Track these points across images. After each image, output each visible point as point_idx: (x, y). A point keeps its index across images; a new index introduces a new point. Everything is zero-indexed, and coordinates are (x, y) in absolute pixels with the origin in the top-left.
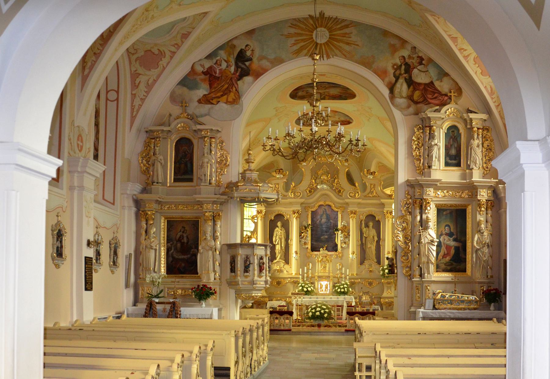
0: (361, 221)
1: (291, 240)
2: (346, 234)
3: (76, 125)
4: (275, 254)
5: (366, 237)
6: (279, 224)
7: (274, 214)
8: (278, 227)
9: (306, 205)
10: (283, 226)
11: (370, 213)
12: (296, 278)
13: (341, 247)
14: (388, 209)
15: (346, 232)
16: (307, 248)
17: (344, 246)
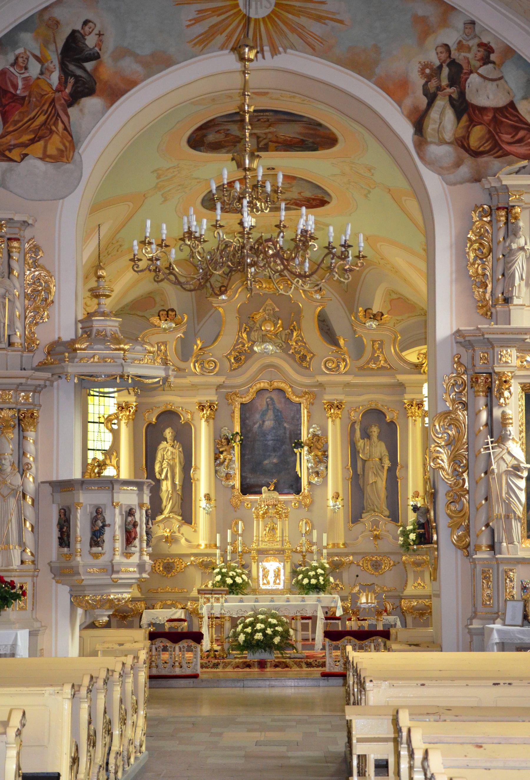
1: (197, 468)
2: (320, 453)
4: (160, 500)
6: (168, 433)
10: (176, 438)
13: (310, 483)
15: (319, 449)
16: (233, 487)
17: (315, 480)
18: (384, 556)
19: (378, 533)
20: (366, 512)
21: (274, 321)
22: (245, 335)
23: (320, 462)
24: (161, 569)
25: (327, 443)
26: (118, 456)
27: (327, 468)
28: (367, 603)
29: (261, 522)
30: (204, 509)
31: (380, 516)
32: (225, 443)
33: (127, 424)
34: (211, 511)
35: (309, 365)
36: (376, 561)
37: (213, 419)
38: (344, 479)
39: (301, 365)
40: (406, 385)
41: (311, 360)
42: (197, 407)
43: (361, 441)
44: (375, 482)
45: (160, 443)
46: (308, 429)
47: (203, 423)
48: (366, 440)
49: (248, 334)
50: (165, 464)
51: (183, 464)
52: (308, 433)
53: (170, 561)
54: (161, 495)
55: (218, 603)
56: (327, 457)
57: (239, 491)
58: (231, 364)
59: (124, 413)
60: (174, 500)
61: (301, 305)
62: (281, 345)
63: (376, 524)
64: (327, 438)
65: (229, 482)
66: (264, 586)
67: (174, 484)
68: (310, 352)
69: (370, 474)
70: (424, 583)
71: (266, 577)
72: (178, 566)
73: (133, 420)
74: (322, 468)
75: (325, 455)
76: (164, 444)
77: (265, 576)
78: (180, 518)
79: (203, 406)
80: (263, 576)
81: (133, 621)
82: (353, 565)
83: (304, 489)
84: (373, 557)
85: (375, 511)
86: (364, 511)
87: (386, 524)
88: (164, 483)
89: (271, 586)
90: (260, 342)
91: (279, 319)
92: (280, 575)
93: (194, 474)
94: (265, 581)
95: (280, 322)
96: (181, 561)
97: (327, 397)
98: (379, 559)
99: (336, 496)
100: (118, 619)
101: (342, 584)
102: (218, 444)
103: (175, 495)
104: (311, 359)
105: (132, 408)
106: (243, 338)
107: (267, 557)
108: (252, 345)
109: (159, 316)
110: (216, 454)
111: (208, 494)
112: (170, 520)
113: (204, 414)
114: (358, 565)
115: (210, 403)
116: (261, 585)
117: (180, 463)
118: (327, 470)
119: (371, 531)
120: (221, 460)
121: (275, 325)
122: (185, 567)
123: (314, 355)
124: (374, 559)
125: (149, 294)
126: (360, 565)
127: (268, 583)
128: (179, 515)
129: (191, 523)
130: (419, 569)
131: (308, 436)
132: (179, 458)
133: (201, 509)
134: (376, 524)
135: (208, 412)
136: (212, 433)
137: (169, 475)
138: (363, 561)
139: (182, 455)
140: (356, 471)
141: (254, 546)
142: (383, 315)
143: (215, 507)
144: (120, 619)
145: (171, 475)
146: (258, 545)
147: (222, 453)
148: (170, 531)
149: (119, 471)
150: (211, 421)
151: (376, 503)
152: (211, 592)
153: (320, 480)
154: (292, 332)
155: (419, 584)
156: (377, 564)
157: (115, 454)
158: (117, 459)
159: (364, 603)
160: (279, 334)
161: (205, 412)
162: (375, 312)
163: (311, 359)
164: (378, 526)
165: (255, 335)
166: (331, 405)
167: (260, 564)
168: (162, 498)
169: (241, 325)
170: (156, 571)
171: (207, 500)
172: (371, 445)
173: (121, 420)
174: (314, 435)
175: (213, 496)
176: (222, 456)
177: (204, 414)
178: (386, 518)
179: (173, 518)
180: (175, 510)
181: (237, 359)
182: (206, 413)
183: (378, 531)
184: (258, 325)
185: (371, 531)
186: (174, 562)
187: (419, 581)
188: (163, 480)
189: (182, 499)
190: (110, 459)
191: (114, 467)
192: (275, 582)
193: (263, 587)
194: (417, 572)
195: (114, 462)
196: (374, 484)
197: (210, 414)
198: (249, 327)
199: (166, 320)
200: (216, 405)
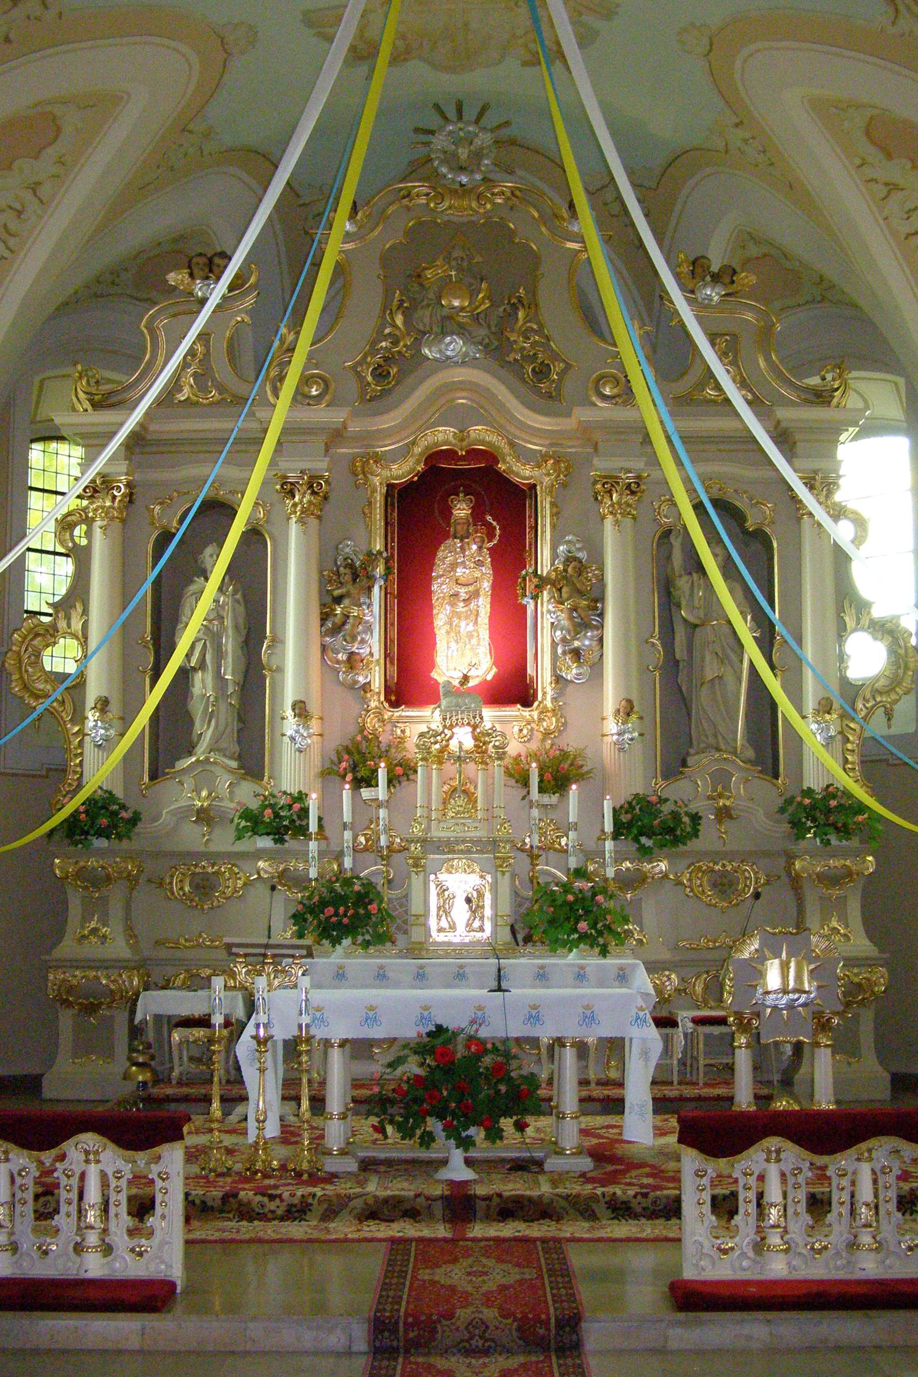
1: (278, 641)
13: (558, 679)
16: (366, 687)
17: (571, 672)
18: (742, 861)
19: (728, 803)
20: (697, 753)
21: (471, 285)
22: (399, 320)
24: (187, 889)
25: (601, 580)
26: (85, 612)
27: (601, 640)
28: (785, 991)
29: (434, 772)
30: (292, 739)
31: (734, 762)
33: (104, 528)
34: (309, 746)
35: (558, 389)
36: (723, 874)
37: (319, 518)
38: (644, 670)
39: (537, 391)
40: (798, 437)
41: (560, 380)
42: (278, 487)
43: (685, 578)
44: (720, 678)
45: (191, 582)
46: (554, 548)
47: (294, 528)
48: (695, 575)
49: (408, 315)
51: (244, 632)
52: (554, 556)
53: (210, 870)
54: (190, 707)
56: (602, 615)
57: (382, 698)
58: (364, 385)
59: (99, 503)
60: (222, 721)
61: (535, 247)
62: (487, 341)
63: (721, 778)
64: (601, 568)
66: (442, 934)
67: (219, 677)
68: (556, 357)
69: (708, 658)
70: (847, 926)
71: (447, 914)
72: (230, 883)
73: (123, 521)
74: (585, 642)
75: (596, 608)
77: (445, 910)
78: (234, 764)
79: (292, 484)
80: (439, 908)
81: (112, 1017)
82: (668, 885)
83: (544, 694)
84: (715, 863)
85: (718, 749)
86: (691, 751)
87: (747, 780)
89: (460, 936)
90: (437, 335)
91: (482, 280)
92: (483, 907)
93: (270, 655)
94: (444, 923)
95: (484, 286)
96: (236, 870)
97: (601, 465)
98: (729, 868)
99: (627, 710)
100: (76, 1012)
101: (641, 931)
102: (330, 581)
103: (223, 707)
104: (562, 374)
105: (119, 488)
106: (394, 325)
107: (450, 860)
108: (418, 344)
109: (190, 267)
110: (323, 605)
111: (301, 702)
112: (208, 767)
113: (295, 505)
114: (679, 883)
115: (310, 477)
116: (434, 933)
117: (236, 627)
118: (602, 646)
119: (710, 798)
120: (338, 620)
121: (473, 294)
122: (245, 884)
123: (568, 367)
124: (717, 868)
125: (175, 240)
126: (681, 883)
127: (453, 927)
128: (231, 758)
130: (836, 892)
131: (552, 564)
132: (235, 617)
133: (286, 740)
134: (721, 778)
135: (305, 500)
136: (315, 551)
137: (208, 657)
138: (691, 873)
139: (241, 609)
140: (674, 653)
141: (417, 831)
142: (734, 272)
144: (80, 1011)
145: (213, 658)
146: (429, 828)
147: (338, 600)
148: (210, 794)
150: (313, 522)
151: (722, 728)
152: (262, 951)
153: (585, 669)
154: (515, 308)
155: (835, 930)
156: (725, 881)
157: (79, 607)
158: (85, 618)
159: (775, 992)
160: (482, 316)
161: (297, 499)
162: (715, 268)
163: (562, 374)
164: (726, 787)
165: (424, 316)
166: (610, 482)
167: (432, 877)
168: (193, 713)
169: (388, 294)
171: (300, 715)
173: (93, 520)
174: (569, 560)
175: (314, 708)
176: (338, 611)
177: (295, 505)
178: (748, 766)
179: (215, 763)
180: (223, 745)
181: (380, 374)
182: (301, 501)
183: (728, 798)
184: (431, 295)
185: (710, 798)
186: (217, 873)
187: (834, 924)
188: (194, 669)
189: (240, 719)
190: (68, 618)
191: (77, 638)
192: (469, 925)
193: (440, 938)
194: (830, 899)
195: (77, 625)
196: (717, 682)
197: (310, 502)
198: (409, 298)
199: (207, 278)
200: (326, 482)
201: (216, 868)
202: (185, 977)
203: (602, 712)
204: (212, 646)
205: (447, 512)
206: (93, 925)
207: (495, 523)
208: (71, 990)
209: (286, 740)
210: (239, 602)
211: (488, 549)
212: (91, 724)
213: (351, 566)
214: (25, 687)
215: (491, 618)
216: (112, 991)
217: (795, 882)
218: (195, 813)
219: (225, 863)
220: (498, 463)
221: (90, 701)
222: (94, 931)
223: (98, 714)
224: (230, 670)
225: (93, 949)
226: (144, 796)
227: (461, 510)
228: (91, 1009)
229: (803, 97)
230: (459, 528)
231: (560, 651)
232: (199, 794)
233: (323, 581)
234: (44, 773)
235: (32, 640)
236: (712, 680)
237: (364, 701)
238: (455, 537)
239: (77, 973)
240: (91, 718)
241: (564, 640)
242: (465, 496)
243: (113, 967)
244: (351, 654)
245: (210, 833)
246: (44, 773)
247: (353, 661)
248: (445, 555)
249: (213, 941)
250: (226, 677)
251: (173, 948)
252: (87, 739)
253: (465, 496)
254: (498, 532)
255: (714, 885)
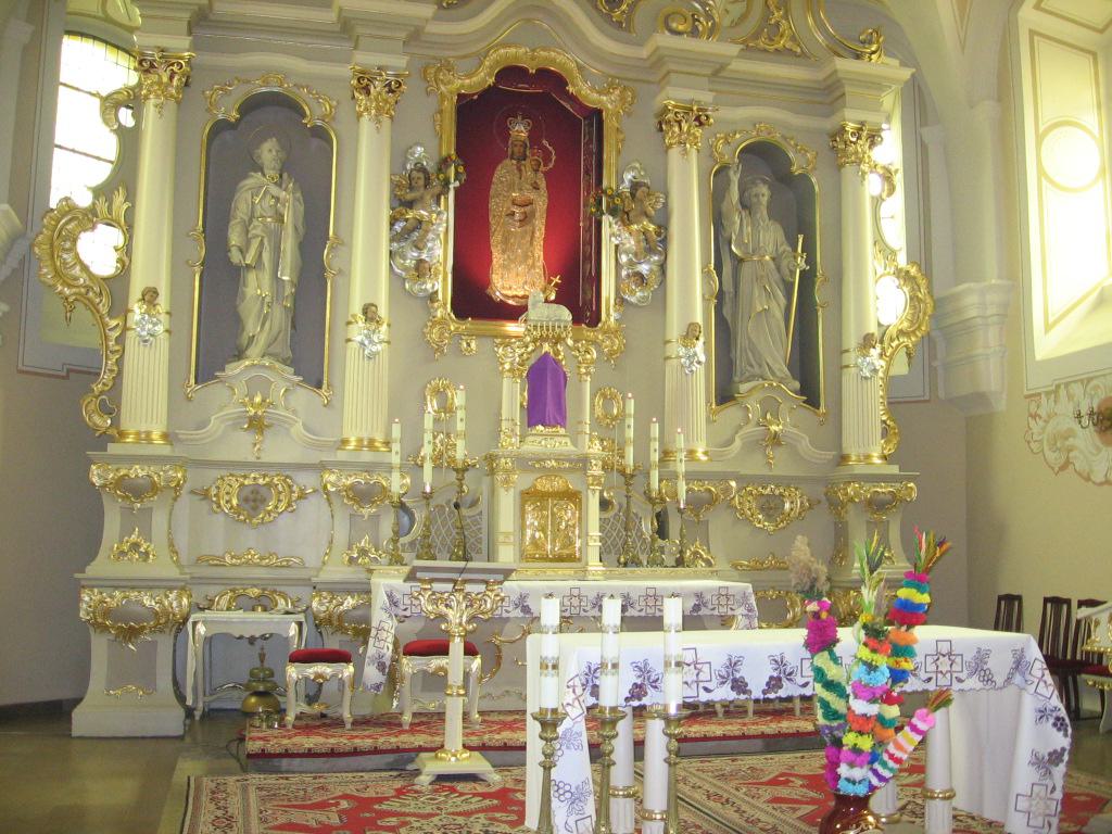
0: (722, 171)
1: (344, 243)
2: (652, 227)
3: (762, 697)
4: (237, 322)
5: (741, 260)
6: (269, 152)
7: (239, 94)
8: (261, 169)
9: (432, 53)
10: (287, 168)
11: (763, 137)
12: (369, 468)
13: (621, 301)
14: (863, 116)
15: (651, 220)
16: (432, 297)
17: (636, 295)
23: (650, 250)
24: (235, 502)
32: (421, 182)
33: (159, 107)
34: (378, 353)
35: (629, 20)
50: (257, 229)
53: (261, 481)
55: (390, 586)
60: (276, 322)
65: (425, 283)
69: (756, 293)
73: (178, 103)
76: (255, 179)
83: (608, 315)
88: (251, 277)
122: (299, 498)
129: (319, 386)
137: (266, 256)
143: (388, 342)
144: (117, 636)
147: (410, 205)
148: (264, 401)
149: (131, 238)
168: (243, 315)
170: (219, 506)
172: (755, 226)
180: (276, 349)
201: (267, 479)
202: (231, 597)
203: (664, 335)
204: (269, 241)
205: (505, 134)
206: (134, 538)
207: (550, 148)
208: (107, 613)
209: (353, 346)
210: (298, 200)
211: (545, 173)
212: (137, 317)
213: (423, 170)
214: (57, 274)
215: (545, 240)
216: (157, 613)
217: (835, 505)
218: (247, 420)
219: (278, 475)
220: (567, 85)
221: (136, 291)
222: (136, 546)
223: (145, 306)
224: (288, 271)
225: (132, 568)
226: (189, 400)
227: (520, 130)
228: (131, 633)
229: (64, 364)
230: (516, 149)
231: (624, 273)
232: (252, 399)
233: (395, 186)
234: (64, 374)
235: (67, 223)
236: (760, 313)
237: (429, 312)
238: (512, 158)
239: (117, 593)
240: (137, 311)
241: (631, 263)
242: (523, 119)
243: (158, 587)
244: (420, 262)
245: (261, 442)
246: (64, 374)
247: (421, 270)
248: (504, 173)
249: (262, 558)
250: (284, 278)
251: (216, 565)
252: (130, 334)
253: (523, 119)
254: (554, 158)
255: (762, 509)
